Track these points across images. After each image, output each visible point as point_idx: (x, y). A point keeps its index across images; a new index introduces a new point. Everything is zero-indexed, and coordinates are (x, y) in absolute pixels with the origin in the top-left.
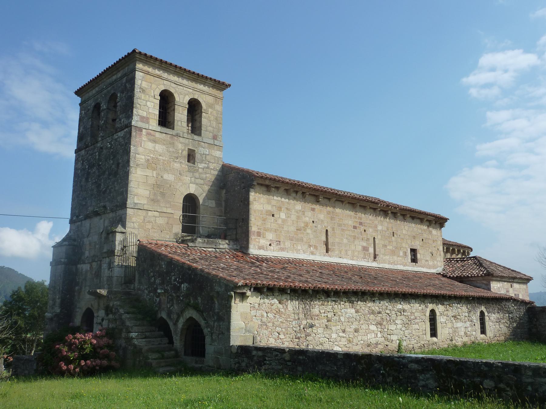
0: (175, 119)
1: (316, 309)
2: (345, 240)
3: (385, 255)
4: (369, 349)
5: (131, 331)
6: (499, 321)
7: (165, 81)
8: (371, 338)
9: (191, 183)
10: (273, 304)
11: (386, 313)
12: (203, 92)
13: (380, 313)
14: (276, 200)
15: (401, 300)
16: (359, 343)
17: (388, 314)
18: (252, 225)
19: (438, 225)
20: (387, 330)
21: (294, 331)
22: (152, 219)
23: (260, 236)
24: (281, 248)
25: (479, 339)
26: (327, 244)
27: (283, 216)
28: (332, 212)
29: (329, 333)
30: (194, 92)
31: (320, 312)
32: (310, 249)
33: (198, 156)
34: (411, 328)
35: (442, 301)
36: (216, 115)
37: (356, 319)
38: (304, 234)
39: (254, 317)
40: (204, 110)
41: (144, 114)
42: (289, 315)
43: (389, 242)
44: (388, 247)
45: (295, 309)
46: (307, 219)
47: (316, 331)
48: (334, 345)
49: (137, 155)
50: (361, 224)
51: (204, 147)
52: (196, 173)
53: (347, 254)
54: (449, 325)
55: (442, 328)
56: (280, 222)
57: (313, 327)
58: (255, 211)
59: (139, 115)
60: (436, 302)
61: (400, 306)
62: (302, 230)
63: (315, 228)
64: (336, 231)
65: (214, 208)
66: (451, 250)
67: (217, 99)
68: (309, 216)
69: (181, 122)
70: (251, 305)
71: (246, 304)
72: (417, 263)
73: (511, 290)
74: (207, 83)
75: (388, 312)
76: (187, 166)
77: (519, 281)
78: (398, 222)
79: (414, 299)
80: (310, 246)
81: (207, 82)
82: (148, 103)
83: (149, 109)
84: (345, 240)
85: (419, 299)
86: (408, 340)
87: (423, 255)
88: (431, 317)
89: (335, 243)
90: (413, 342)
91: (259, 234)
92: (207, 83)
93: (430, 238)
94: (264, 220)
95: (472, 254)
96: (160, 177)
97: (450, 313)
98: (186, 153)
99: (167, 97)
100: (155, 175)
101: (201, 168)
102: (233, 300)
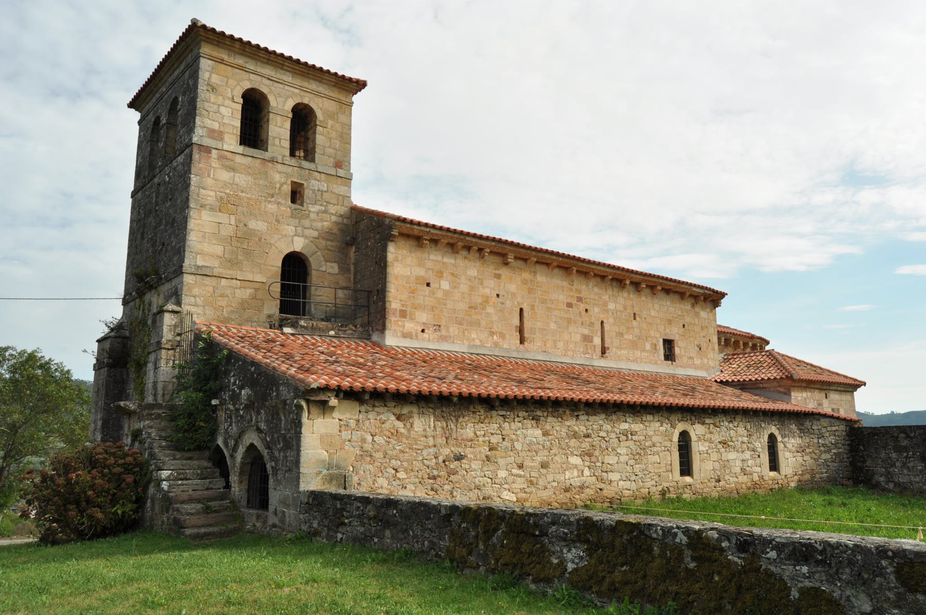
0: (270, 134)
1: (467, 430)
2: (552, 324)
3: (620, 348)
4: (568, 496)
5: (163, 468)
6: (801, 450)
7: (251, 75)
8: (572, 477)
9: (295, 235)
10: (385, 420)
11: (599, 436)
12: (318, 94)
13: (588, 436)
14: (433, 260)
15: (627, 415)
16: (549, 486)
17: (604, 438)
18: (391, 299)
19: (709, 305)
20: (600, 464)
21: (425, 465)
22: (228, 292)
23: (405, 317)
24: (442, 336)
25: (766, 478)
26: (521, 330)
27: (445, 285)
28: (531, 281)
29: (492, 469)
30: (303, 93)
31: (475, 434)
32: (493, 337)
33: (308, 193)
34: (645, 461)
35: (701, 417)
36: (341, 130)
37: (543, 447)
38: (481, 314)
39: (347, 443)
40: (320, 121)
41: (216, 126)
42: (416, 440)
43: (628, 328)
44: (626, 337)
45: (428, 429)
46: (487, 291)
47: (467, 466)
48: (502, 490)
49: (201, 190)
50: (580, 299)
51: (319, 179)
52: (305, 219)
53: (555, 346)
54: (715, 456)
55: (702, 461)
56: (440, 294)
57: (462, 459)
58: (396, 278)
59: (205, 127)
60: (691, 419)
61: (624, 426)
62: (479, 308)
63: (501, 305)
64: (536, 311)
65: (336, 274)
66: (732, 342)
67: (344, 106)
68: (490, 287)
69: (280, 139)
70: (342, 423)
71: (331, 420)
72: (675, 361)
73: (825, 403)
74: (324, 79)
75: (602, 434)
76: (289, 209)
77: (839, 389)
78: (643, 298)
79: (650, 414)
80: (492, 334)
81: (324, 77)
82: (222, 109)
83: (223, 118)
84: (552, 324)
85: (660, 415)
86: (640, 480)
87: (685, 349)
88: (681, 443)
89: (535, 329)
90: (649, 483)
91: (403, 314)
92: (324, 79)
93: (697, 322)
94: (413, 292)
95: (767, 348)
96: (242, 225)
97: (717, 438)
98: (287, 189)
99: (259, 101)
100: (233, 222)
101: (314, 212)
102: (305, 415)
